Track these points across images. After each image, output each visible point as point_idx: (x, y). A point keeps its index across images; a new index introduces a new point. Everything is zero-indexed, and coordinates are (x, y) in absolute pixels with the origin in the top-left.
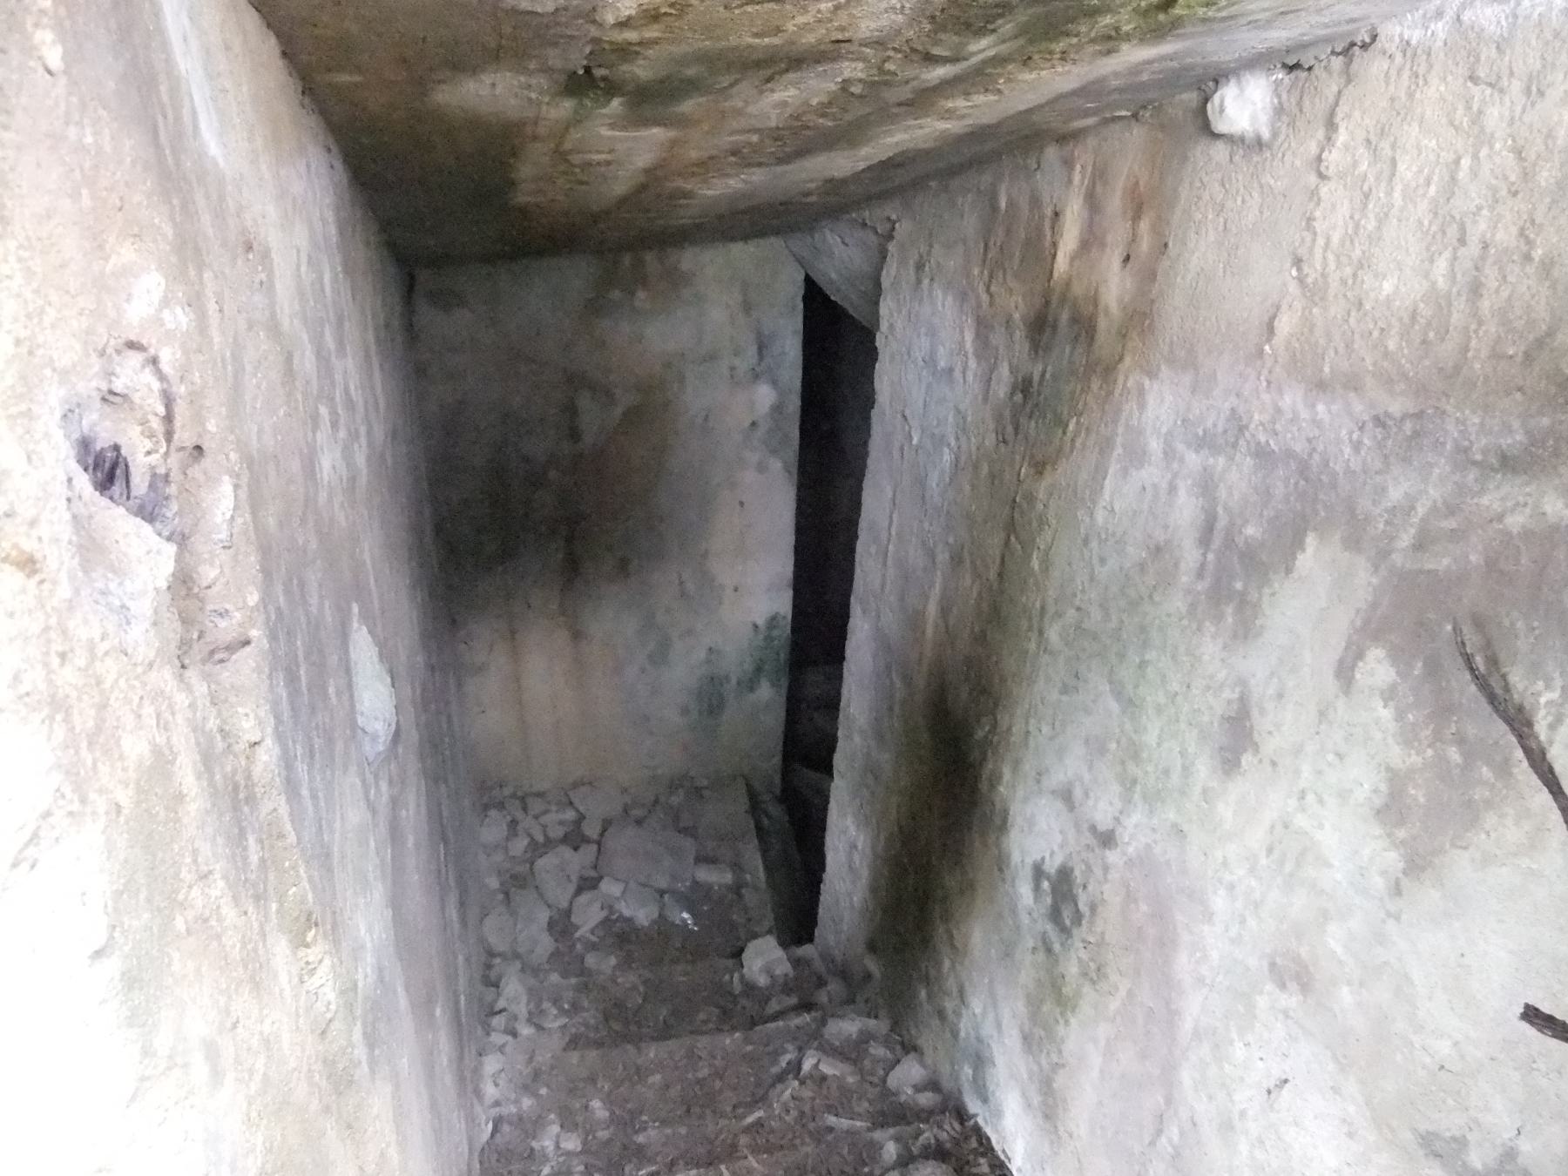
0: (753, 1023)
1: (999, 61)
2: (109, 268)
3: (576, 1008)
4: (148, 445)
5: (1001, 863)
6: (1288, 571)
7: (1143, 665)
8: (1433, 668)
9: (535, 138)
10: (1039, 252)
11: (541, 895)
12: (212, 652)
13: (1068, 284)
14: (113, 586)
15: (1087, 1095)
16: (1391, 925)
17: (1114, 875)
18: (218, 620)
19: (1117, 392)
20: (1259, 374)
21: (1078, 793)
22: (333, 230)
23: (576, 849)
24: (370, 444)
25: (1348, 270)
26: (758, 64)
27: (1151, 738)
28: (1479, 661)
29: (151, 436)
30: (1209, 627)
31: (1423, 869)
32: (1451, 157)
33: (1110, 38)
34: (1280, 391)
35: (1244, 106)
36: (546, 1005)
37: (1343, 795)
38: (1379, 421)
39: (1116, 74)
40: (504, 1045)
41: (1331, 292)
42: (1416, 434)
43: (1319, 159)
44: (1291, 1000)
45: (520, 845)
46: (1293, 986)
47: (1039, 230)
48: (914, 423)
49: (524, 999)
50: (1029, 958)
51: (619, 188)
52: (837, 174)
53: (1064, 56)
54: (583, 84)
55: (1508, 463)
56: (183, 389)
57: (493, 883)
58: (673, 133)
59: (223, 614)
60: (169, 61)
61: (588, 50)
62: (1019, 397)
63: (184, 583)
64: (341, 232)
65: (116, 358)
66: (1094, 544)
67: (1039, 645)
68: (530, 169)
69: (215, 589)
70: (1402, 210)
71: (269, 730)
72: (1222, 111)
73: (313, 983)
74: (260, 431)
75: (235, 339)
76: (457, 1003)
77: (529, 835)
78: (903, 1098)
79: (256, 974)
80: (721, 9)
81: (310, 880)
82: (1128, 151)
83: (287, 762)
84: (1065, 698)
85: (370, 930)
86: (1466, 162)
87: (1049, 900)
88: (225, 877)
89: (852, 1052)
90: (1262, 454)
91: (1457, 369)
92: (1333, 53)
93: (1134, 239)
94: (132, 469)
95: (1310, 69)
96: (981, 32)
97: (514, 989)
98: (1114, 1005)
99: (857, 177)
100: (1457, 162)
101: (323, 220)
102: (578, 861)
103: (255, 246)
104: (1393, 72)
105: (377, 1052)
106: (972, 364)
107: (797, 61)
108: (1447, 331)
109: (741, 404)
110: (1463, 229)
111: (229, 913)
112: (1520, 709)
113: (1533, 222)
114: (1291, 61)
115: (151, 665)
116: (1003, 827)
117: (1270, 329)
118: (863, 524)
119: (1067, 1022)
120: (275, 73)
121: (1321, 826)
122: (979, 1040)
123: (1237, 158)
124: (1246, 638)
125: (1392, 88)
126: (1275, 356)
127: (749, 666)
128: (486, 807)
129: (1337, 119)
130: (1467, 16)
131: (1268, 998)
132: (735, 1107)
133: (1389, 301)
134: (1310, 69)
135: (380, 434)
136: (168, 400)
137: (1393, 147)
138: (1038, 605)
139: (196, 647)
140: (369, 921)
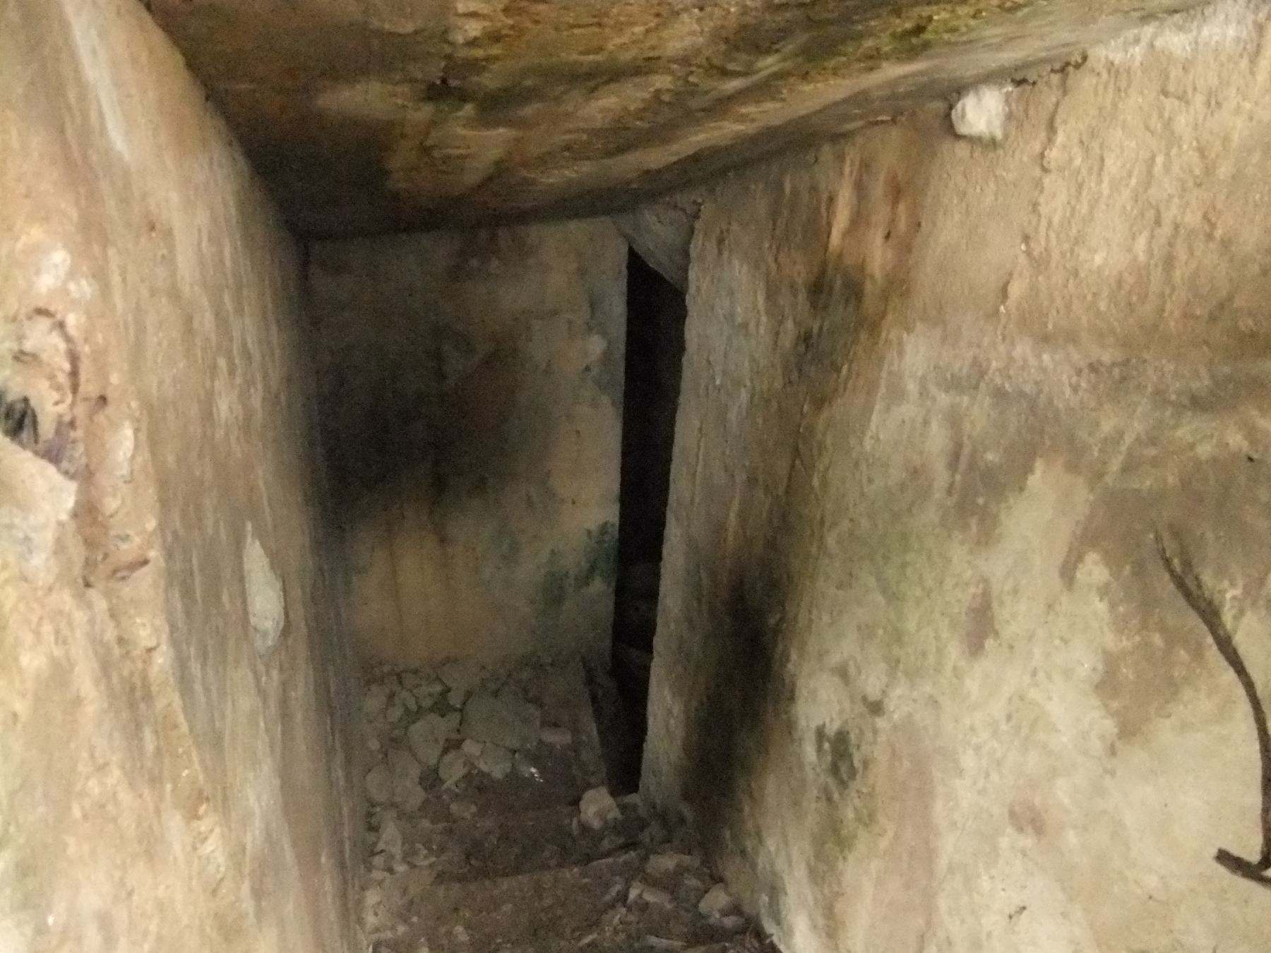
0: (588, 859)
1: (781, 75)
2: (19, 245)
3: (442, 849)
4: (55, 396)
5: (790, 726)
6: (1021, 489)
7: (904, 565)
8: (1139, 570)
9: (403, 136)
10: (817, 230)
11: (414, 755)
12: (115, 572)
13: (840, 255)
14: (17, 521)
15: (862, 919)
16: (1108, 781)
17: (882, 738)
18: (119, 543)
19: (881, 342)
20: (996, 329)
21: (852, 670)
22: (233, 211)
23: (443, 716)
24: (267, 388)
25: (1066, 246)
26: (590, 75)
27: (911, 625)
28: (1176, 562)
29: (58, 388)
30: (957, 535)
31: (1133, 734)
32: (1148, 155)
33: (871, 57)
34: (1013, 344)
35: (982, 112)
36: (419, 846)
37: (1068, 673)
38: (1093, 368)
39: (879, 87)
40: (383, 881)
41: (1053, 265)
42: (1123, 379)
43: (1042, 155)
44: (1027, 841)
45: (396, 713)
46: (1029, 829)
47: (818, 209)
48: (718, 368)
49: (399, 842)
50: (814, 806)
51: (472, 178)
52: (653, 166)
53: (835, 72)
54: (440, 92)
55: (1197, 403)
56: (87, 349)
57: (374, 745)
58: (520, 134)
59: (126, 538)
60: (77, 70)
61: (443, 64)
62: (802, 348)
63: (88, 513)
64: (242, 212)
65: (26, 323)
66: (863, 467)
67: (819, 548)
68: (399, 160)
69: (120, 516)
70: (1110, 196)
71: (165, 637)
72: (963, 116)
73: (209, 847)
74: (161, 383)
75: (137, 303)
76: (341, 852)
77: (404, 705)
78: (712, 921)
79: (150, 847)
80: (552, 32)
81: (202, 762)
82: (889, 149)
83: (181, 663)
84: (841, 593)
85: (258, 799)
86: (1160, 160)
87: (829, 758)
88: (122, 768)
89: (669, 884)
90: (999, 395)
91: (1156, 327)
92: (1053, 71)
93: (893, 221)
94: (40, 418)
95: (1034, 83)
96: (768, 52)
97: (391, 833)
98: (884, 843)
99: (669, 168)
100: (1153, 158)
101: (226, 205)
102: (443, 726)
103: (158, 226)
104: (1101, 88)
105: (263, 904)
106: (764, 319)
107: (613, 74)
108: (1146, 295)
109: (579, 352)
110: (1158, 212)
111: (125, 797)
112: (1210, 603)
113: (1214, 208)
114: (1018, 77)
115: (50, 589)
116: (792, 699)
117: (1004, 293)
118: (676, 450)
119: (845, 859)
120: (178, 80)
121: (1050, 698)
122: (774, 874)
123: (976, 154)
124: (987, 544)
125: (1100, 99)
126: (1008, 314)
127: (585, 565)
128: (368, 683)
129: (1058, 121)
130: (1159, 43)
131: (1008, 839)
132: (573, 931)
133: (1100, 270)
134: (1034, 83)
135: (276, 376)
136: (74, 358)
137: (1101, 146)
138: (818, 517)
139: (101, 567)
140: (258, 792)
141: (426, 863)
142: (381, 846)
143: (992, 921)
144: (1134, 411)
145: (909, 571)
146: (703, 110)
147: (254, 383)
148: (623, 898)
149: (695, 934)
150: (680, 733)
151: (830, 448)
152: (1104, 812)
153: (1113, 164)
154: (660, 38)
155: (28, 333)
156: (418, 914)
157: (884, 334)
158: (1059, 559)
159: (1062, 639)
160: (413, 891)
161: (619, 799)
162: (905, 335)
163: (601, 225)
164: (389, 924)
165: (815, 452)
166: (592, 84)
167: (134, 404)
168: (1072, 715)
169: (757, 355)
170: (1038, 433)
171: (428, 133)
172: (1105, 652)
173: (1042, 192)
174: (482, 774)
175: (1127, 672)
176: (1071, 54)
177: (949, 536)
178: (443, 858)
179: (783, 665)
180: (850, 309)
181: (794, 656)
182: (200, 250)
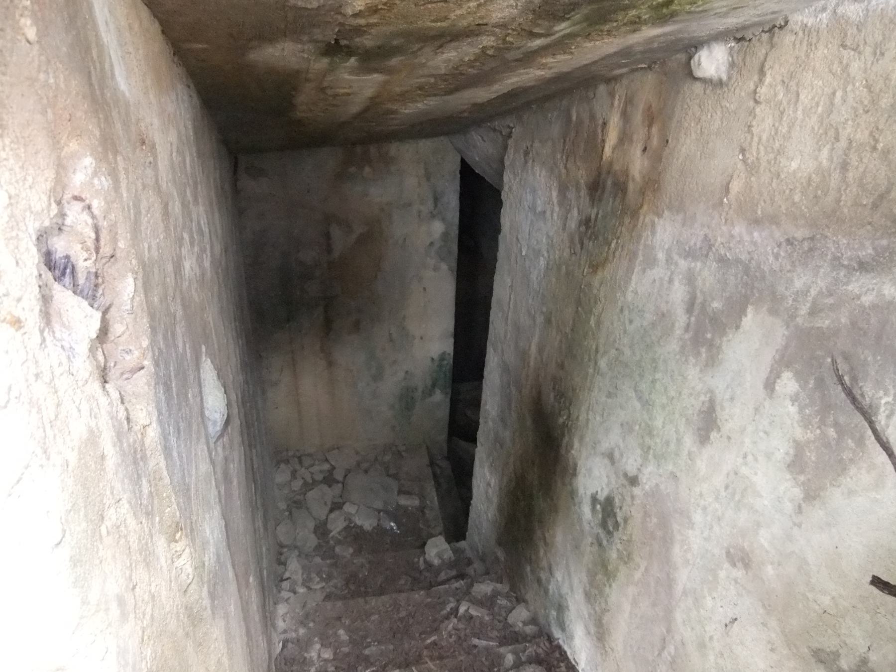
1: (572, 36)
3: (330, 577)
4: (85, 255)
5: (573, 494)
6: (738, 327)
7: (654, 381)
8: (820, 383)
9: (307, 80)
10: (595, 145)
11: (310, 513)
12: (122, 374)
13: (611, 164)
17: (637, 502)
21: (617, 454)
25: (772, 156)
26: (434, 38)
27: (658, 423)
28: (846, 378)
29: (87, 250)
30: (692, 360)
33: (635, 23)
34: (733, 225)
35: (712, 62)
36: (313, 575)
37: (769, 456)
38: (789, 242)
39: (638, 43)
40: (289, 598)
42: (811, 250)
43: (755, 92)
44: (739, 573)
45: (297, 485)
46: (739, 565)
49: (300, 572)
50: (588, 549)
51: (354, 109)
52: (479, 101)
54: (334, 49)
55: (863, 266)
57: (282, 505)
58: (388, 77)
62: (583, 229)
66: (626, 313)
71: (155, 418)
72: (699, 64)
73: (180, 562)
74: (150, 248)
78: (517, 629)
80: (413, 6)
82: (646, 87)
83: (165, 436)
84: (609, 401)
85: (212, 532)
86: (839, 94)
87: (600, 516)
88: (130, 503)
89: (488, 602)
90: (722, 260)
93: (649, 137)
95: (750, 40)
96: (563, 19)
97: (294, 567)
98: (638, 575)
99: (490, 102)
100: (834, 94)
104: (798, 42)
106: (557, 209)
109: (424, 232)
111: (132, 522)
113: (877, 129)
114: (739, 36)
116: (574, 474)
117: (727, 190)
119: (610, 586)
120: (158, 44)
121: (756, 474)
122: (561, 596)
123: (708, 92)
124: (713, 366)
127: (429, 383)
128: (278, 463)
129: (767, 67)
130: (840, 10)
131: (725, 572)
134: (750, 40)
135: (218, 248)
137: (797, 85)
138: (594, 347)
140: (211, 528)
141: (318, 587)
142: (287, 575)
143: (713, 629)
144: (818, 272)
145: (658, 385)
146: (516, 60)
147: (205, 251)
148: (455, 611)
149: (505, 637)
150: (495, 500)
151: (603, 300)
152: (793, 552)
153: (805, 97)
154: (488, 10)
155: (68, 213)
156: (314, 621)
157: (641, 218)
158: (764, 373)
159: (766, 433)
160: (312, 604)
161: (452, 544)
162: (656, 219)
163: (442, 142)
164: (294, 628)
165: (592, 301)
166: (437, 43)
167: (134, 262)
168: (771, 486)
169: (551, 234)
170: (751, 289)
171: (324, 76)
172: (795, 441)
173: (754, 117)
174: (356, 526)
175: (811, 456)
176: (777, 19)
177: (686, 360)
178: (331, 584)
179: (568, 451)
180: (618, 200)
181: (576, 444)
182: (172, 159)
